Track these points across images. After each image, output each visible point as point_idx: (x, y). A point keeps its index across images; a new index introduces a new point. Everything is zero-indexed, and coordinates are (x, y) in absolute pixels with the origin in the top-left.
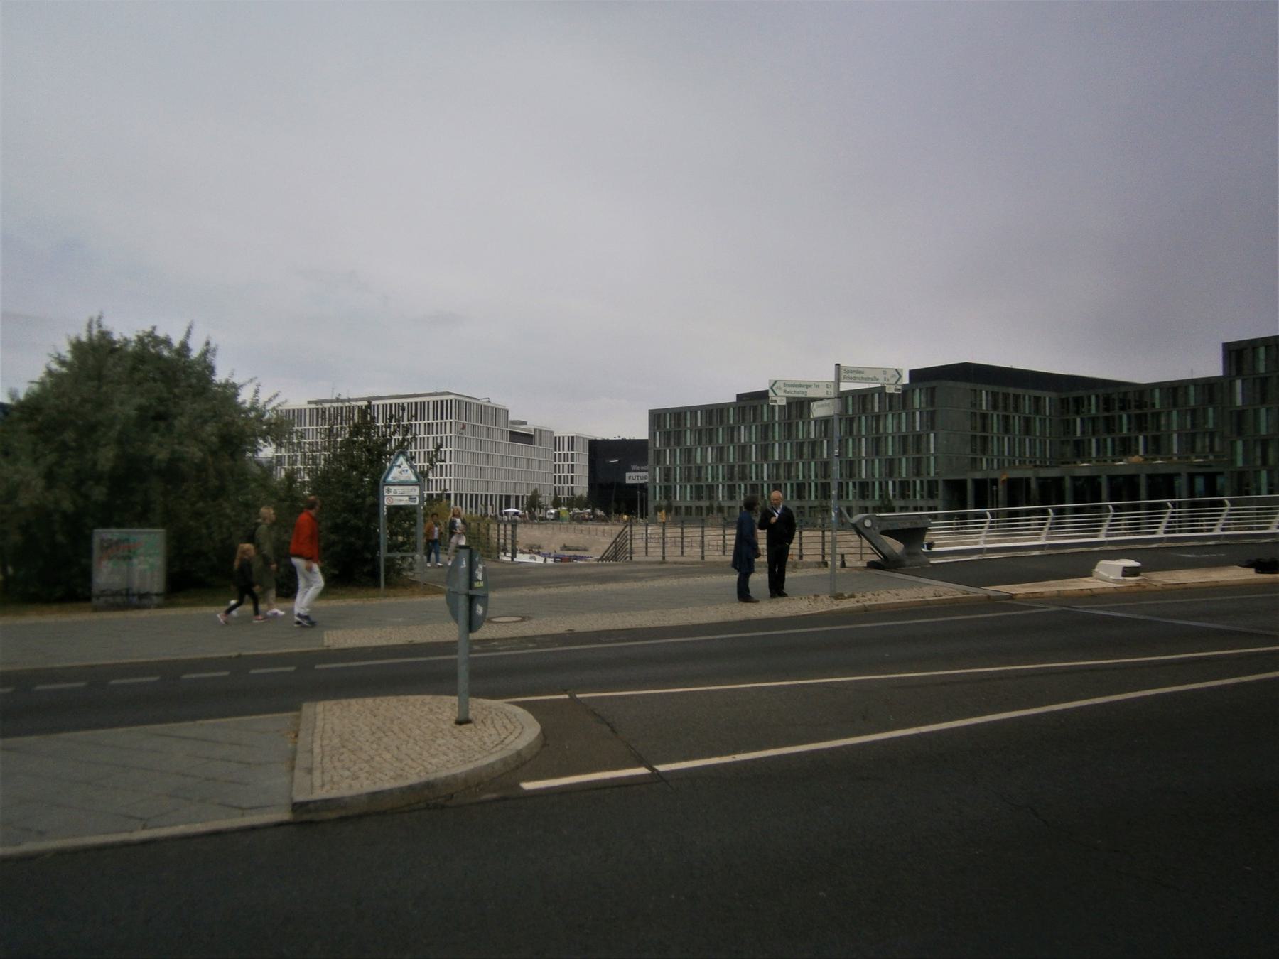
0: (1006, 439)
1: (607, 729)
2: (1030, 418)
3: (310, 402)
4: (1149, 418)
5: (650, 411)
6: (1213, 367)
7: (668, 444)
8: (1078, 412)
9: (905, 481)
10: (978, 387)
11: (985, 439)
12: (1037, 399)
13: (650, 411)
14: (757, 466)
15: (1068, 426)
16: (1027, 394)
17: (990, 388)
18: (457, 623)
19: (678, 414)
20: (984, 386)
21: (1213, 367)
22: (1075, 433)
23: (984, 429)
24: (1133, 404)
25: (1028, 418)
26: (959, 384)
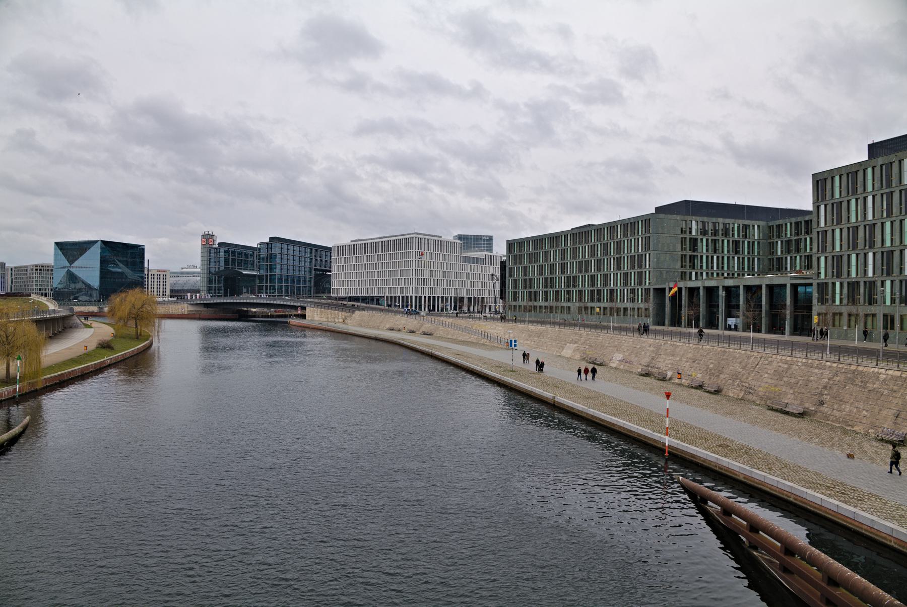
0: (736, 258)
1: (898, 473)
2: (739, 241)
3: (351, 241)
4: (793, 242)
5: (508, 241)
6: (268, 240)
7: (789, 252)
8: (779, 236)
9: (823, 283)
10: (689, 218)
11: (693, 258)
12: (746, 227)
13: (508, 241)
14: (743, 268)
15: (772, 246)
16: (735, 224)
17: (699, 219)
18: (97, 348)
19: (521, 243)
20: (694, 217)
21: (268, 240)
22: (777, 253)
23: (695, 250)
24: (720, 232)
25: (736, 241)
26: (670, 216)
